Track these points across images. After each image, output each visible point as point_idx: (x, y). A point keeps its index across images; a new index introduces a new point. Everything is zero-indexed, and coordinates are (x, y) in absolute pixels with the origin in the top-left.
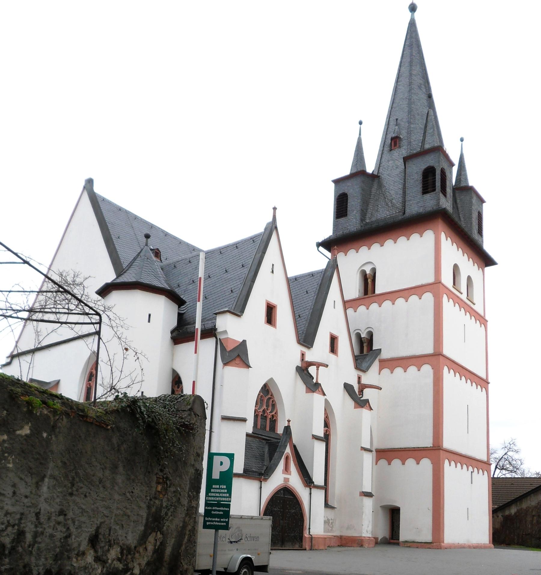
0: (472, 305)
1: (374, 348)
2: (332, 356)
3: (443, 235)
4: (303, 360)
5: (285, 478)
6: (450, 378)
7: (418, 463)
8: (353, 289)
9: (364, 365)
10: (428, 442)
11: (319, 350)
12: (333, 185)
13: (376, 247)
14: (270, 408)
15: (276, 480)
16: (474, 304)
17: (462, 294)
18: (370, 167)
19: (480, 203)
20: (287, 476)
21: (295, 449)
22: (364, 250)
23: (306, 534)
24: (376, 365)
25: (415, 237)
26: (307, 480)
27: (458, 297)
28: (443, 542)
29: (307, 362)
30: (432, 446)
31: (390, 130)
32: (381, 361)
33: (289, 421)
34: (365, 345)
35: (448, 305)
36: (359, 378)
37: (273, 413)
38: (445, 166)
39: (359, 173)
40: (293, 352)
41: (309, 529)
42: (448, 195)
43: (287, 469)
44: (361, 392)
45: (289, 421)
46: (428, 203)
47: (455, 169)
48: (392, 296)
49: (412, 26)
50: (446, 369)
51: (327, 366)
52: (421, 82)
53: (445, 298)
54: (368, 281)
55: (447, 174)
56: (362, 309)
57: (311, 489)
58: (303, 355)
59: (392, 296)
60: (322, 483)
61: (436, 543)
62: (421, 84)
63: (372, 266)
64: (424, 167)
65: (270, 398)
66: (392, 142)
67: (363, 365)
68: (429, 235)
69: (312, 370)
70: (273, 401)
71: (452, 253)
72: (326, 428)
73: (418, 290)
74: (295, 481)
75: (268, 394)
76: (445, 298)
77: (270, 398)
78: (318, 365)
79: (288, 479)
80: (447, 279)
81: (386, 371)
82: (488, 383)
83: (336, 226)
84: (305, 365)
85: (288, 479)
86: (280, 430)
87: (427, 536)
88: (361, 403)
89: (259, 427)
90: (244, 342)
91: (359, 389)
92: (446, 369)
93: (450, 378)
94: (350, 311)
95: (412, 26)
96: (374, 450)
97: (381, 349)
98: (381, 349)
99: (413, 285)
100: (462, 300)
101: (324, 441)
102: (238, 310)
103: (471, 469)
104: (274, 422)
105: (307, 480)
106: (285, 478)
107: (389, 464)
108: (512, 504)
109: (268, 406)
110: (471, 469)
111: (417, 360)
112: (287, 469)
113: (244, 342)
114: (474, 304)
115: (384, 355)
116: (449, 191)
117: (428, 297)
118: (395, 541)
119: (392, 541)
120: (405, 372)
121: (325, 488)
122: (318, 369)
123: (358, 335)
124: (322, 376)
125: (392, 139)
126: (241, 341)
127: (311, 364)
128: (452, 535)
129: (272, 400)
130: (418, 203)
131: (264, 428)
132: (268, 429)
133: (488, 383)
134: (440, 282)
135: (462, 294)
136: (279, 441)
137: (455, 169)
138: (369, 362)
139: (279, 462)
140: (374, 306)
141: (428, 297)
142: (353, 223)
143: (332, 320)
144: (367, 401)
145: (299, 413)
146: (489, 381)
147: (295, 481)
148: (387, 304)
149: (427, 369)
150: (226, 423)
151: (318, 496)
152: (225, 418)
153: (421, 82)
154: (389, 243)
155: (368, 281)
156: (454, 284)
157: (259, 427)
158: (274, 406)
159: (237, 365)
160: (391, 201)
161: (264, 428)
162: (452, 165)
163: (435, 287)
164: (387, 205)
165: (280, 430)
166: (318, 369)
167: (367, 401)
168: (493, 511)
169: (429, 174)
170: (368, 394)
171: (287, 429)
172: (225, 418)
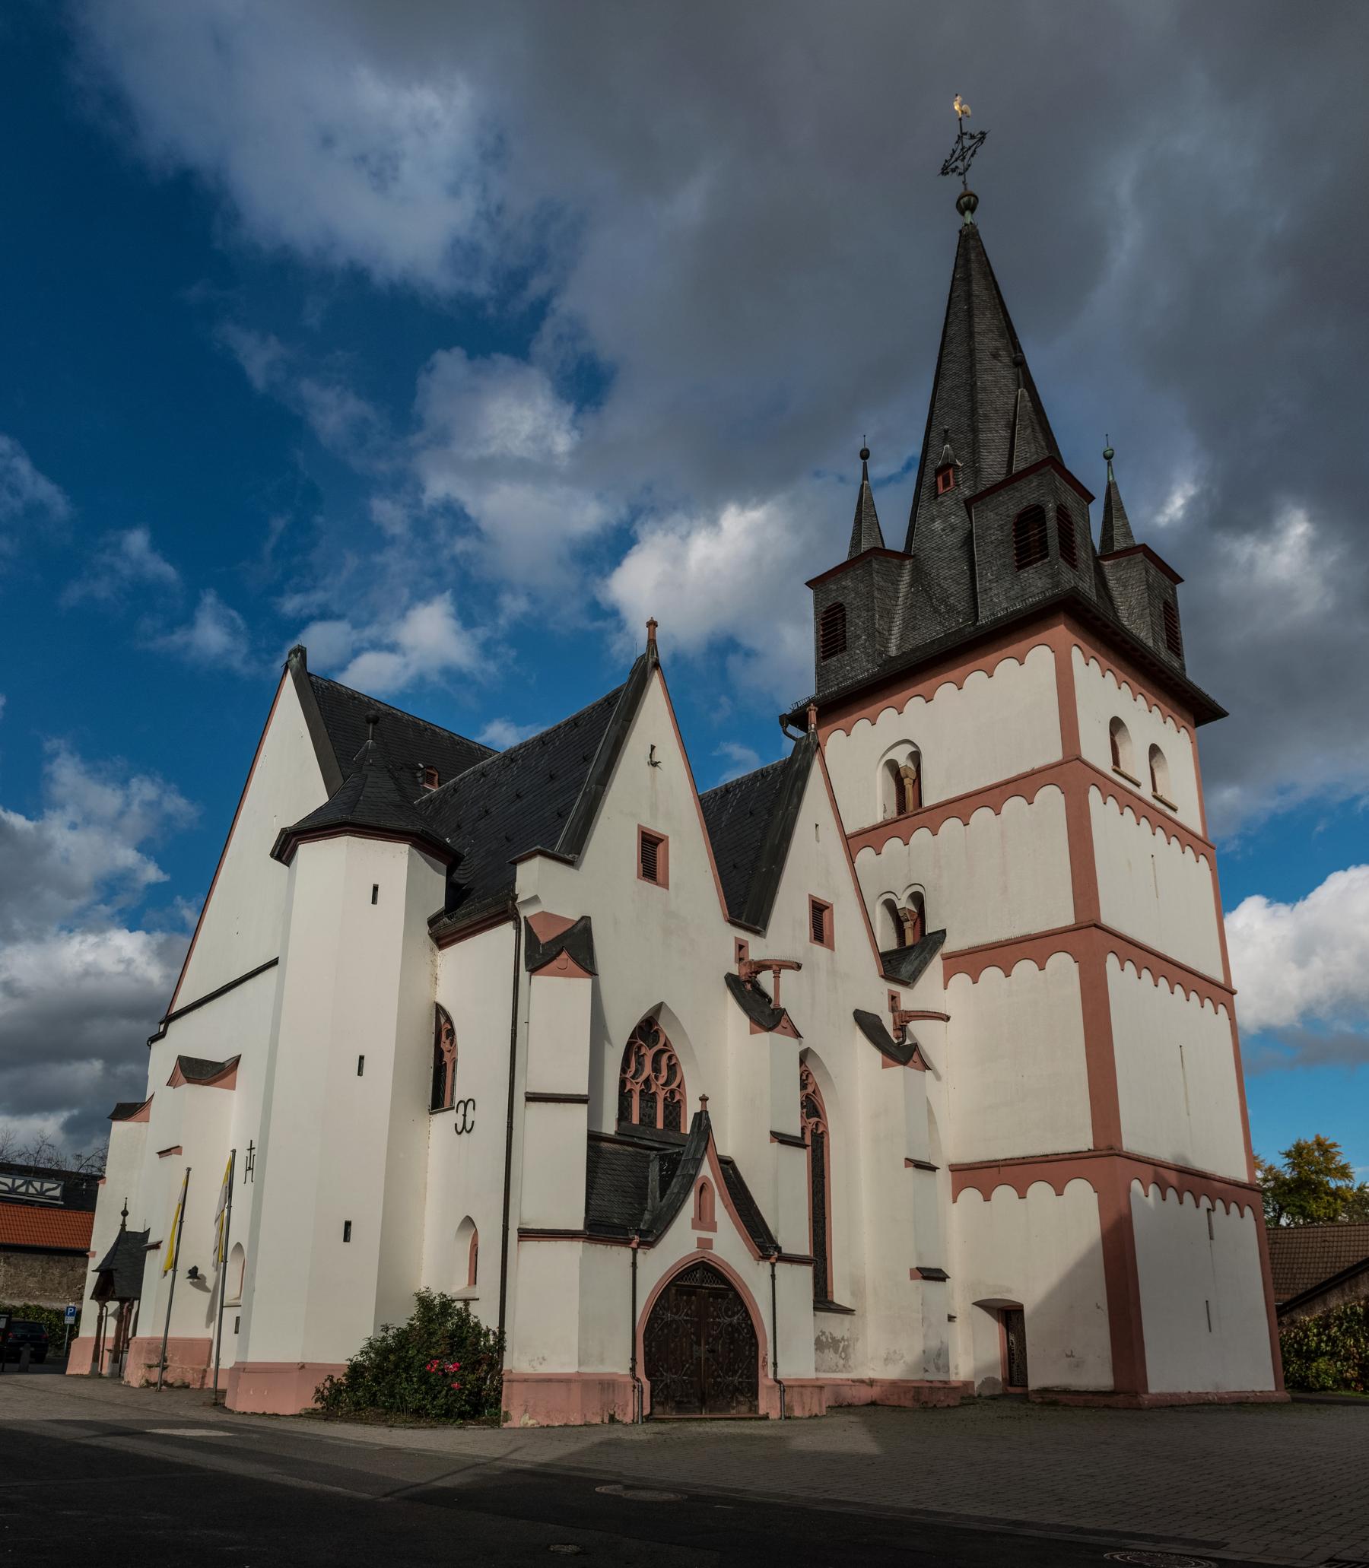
0: (1169, 812)
1: (929, 930)
2: (818, 948)
3: (1076, 654)
4: (741, 959)
5: (699, 1239)
6: (1122, 980)
7: (1059, 1193)
8: (870, 800)
9: (905, 970)
10: (1084, 1141)
11: (786, 929)
12: (810, 594)
13: (915, 705)
14: (664, 1073)
15: (680, 1242)
16: (1174, 810)
17: (1138, 785)
18: (894, 538)
19: (1168, 582)
20: (705, 1235)
21: (727, 1166)
22: (888, 716)
23: (766, 1379)
24: (936, 967)
25: (1007, 668)
26: (762, 1240)
27: (1130, 792)
28: (1146, 1392)
29: (751, 963)
30: (1091, 1147)
31: (931, 456)
32: (946, 958)
33: (704, 1099)
34: (907, 925)
35: (1103, 812)
36: (893, 998)
37: (674, 1086)
38: (1070, 499)
39: (867, 556)
40: (718, 942)
41: (775, 1364)
42: (1081, 566)
43: (703, 1220)
44: (902, 1029)
45: (704, 1099)
46: (1036, 584)
47: (1096, 512)
48: (962, 806)
49: (969, 243)
50: (1112, 961)
51: (799, 967)
52: (998, 344)
53: (1094, 794)
54: (905, 781)
55: (1077, 519)
56: (894, 845)
57: (773, 1265)
58: (741, 947)
59: (962, 806)
60: (805, 1249)
61: (1126, 1393)
62: (997, 349)
63: (911, 749)
64: (1014, 510)
65: (660, 1052)
66: (933, 475)
67: (903, 970)
68: (1040, 658)
69: (765, 979)
70: (670, 1058)
71: (1103, 691)
72: (814, 1120)
73: (1025, 785)
74: (729, 1246)
75: (656, 1041)
76: (1094, 794)
77: (660, 1052)
78: (778, 967)
79: (710, 1241)
80: (1095, 749)
81: (961, 980)
82: (1233, 993)
83: (821, 674)
84: (746, 970)
85: (710, 1241)
86: (687, 1127)
87: (1098, 1375)
88: (900, 1051)
89: (635, 1120)
90: (586, 919)
91: (895, 1022)
92: (1112, 961)
93: (1122, 980)
94: (865, 856)
95: (969, 243)
96: (942, 1163)
97: (944, 931)
98: (944, 931)
99: (1013, 774)
100: (1140, 799)
101: (804, 1146)
102: (570, 853)
103: (1205, 1202)
104: (674, 1109)
105: (762, 1240)
106: (699, 1239)
107: (1022, 1196)
108: (1330, 1289)
109: (656, 1069)
110: (1205, 1202)
111: (1035, 947)
112: (703, 1220)
113: (586, 919)
114: (1174, 810)
115: (950, 945)
116: (1082, 555)
117: (1051, 798)
118: (1018, 1390)
119: (1011, 1390)
120: (1007, 976)
121: (819, 1260)
122: (777, 977)
123: (890, 905)
124: (788, 992)
125: (938, 471)
126: (577, 918)
127: (762, 966)
128: (1168, 1373)
129: (665, 1057)
130: (1007, 591)
131: (648, 1119)
132: (660, 1125)
133: (1233, 993)
134: (1079, 759)
135: (1138, 785)
136: (681, 1149)
137: (1096, 512)
138: (916, 963)
139: (683, 1201)
140: (922, 836)
141: (1051, 798)
142: (858, 666)
143: (813, 861)
144: (915, 1047)
145: (733, 1080)
146: (1235, 986)
147: (729, 1246)
148: (951, 826)
149: (1063, 965)
150: (535, 1106)
151: (797, 1281)
152: (532, 1098)
153: (998, 344)
154: (946, 692)
155: (905, 781)
156: (1116, 761)
157: (635, 1120)
158: (673, 1068)
159: (563, 973)
160: (944, 601)
161: (648, 1119)
162: (1090, 498)
163: (1070, 774)
164: (936, 611)
165: (687, 1127)
166: (777, 977)
167: (1345, 1167)
168: (1278, 1308)
169: (1030, 520)
170: (918, 1030)
171: (702, 1121)
172: (532, 1098)
